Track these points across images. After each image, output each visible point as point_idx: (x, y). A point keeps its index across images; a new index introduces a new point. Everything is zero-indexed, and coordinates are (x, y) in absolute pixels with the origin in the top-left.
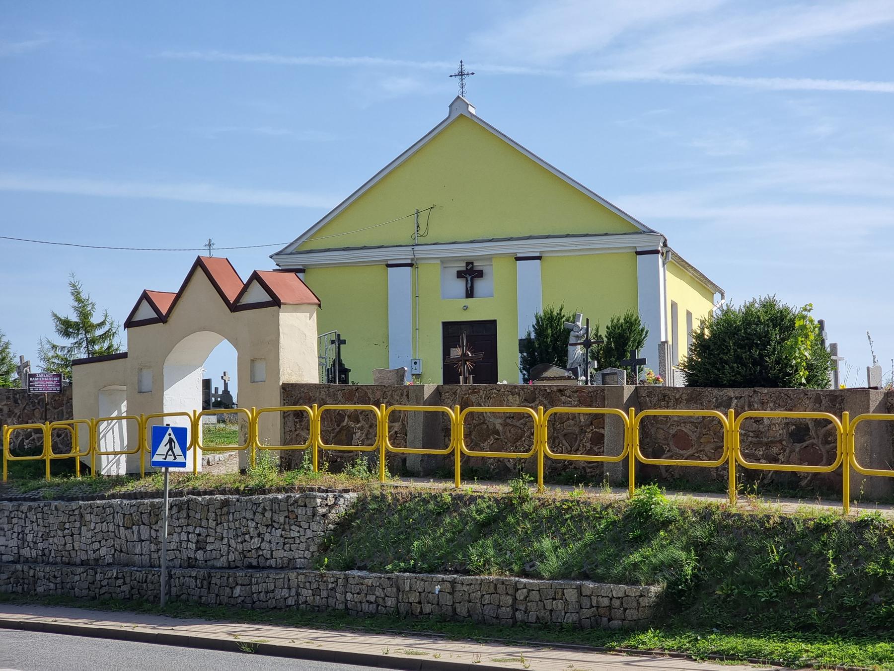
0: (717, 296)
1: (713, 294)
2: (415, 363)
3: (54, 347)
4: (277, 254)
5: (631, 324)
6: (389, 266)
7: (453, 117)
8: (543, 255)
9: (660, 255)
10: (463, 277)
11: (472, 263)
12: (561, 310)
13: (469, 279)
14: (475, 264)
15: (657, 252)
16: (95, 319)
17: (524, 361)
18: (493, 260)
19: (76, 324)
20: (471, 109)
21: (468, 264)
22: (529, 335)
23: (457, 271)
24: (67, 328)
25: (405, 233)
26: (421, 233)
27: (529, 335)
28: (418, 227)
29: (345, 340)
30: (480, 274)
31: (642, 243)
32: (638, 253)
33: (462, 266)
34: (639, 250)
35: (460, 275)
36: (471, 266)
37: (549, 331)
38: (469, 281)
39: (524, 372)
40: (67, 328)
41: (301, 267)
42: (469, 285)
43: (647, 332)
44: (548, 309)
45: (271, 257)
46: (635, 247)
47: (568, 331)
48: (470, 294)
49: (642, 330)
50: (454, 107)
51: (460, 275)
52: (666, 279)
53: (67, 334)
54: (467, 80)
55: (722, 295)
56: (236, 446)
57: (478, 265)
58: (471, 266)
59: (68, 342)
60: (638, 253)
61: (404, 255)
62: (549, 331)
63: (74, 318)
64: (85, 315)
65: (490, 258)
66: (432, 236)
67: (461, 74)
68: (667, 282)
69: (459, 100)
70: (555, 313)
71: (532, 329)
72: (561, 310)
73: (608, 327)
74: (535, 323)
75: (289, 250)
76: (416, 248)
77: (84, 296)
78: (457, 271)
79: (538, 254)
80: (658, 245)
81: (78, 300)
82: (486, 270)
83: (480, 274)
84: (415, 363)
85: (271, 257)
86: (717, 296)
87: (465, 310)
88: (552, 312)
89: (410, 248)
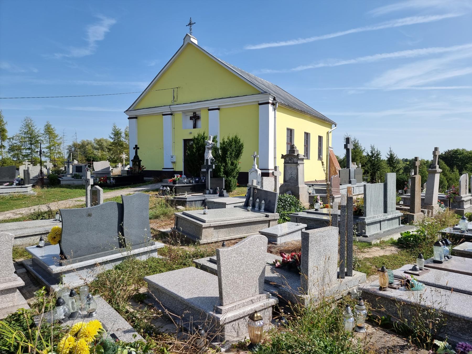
0: (333, 125)
1: (332, 125)
2: (172, 157)
4: (127, 111)
6: (209, 110)
8: (220, 108)
9: (270, 105)
10: (192, 119)
11: (196, 113)
13: (194, 120)
14: (197, 113)
18: (201, 111)
21: (194, 113)
23: (190, 117)
25: (169, 100)
26: (175, 100)
28: (174, 97)
31: (261, 98)
33: (191, 114)
35: (191, 118)
36: (195, 114)
38: (194, 121)
41: (135, 116)
42: (194, 123)
45: (124, 112)
46: (258, 101)
48: (195, 127)
52: (276, 117)
55: (336, 125)
56: (146, 178)
58: (195, 114)
60: (260, 104)
61: (167, 110)
67: (190, 24)
68: (276, 119)
69: (187, 36)
75: (131, 109)
76: (171, 106)
78: (190, 117)
79: (217, 107)
80: (269, 99)
84: (172, 157)
85: (124, 112)
86: (333, 125)
87: (190, 134)
89: (168, 107)
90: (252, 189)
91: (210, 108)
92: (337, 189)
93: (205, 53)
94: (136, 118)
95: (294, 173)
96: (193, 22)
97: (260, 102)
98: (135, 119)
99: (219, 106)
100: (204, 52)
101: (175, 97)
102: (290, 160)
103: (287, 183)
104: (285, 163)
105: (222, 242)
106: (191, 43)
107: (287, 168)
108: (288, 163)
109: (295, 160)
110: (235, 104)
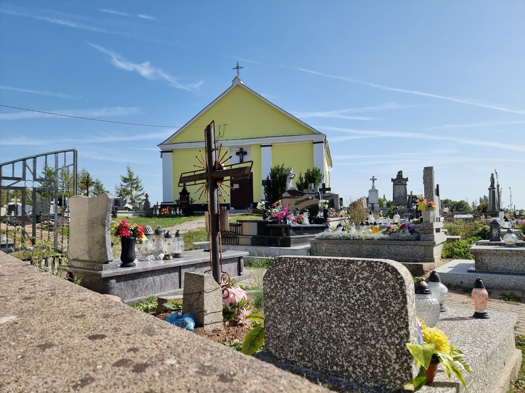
3: (122, 185)
5: (317, 172)
6: (262, 146)
7: (235, 85)
11: (242, 149)
12: (283, 166)
15: (322, 142)
16: (134, 177)
17: (266, 189)
19: (128, 179)
20: (241, 82)
21: (241, 149)
22: (268, 177)
24: (125, 180)
26: (221, 136)
27: (268, 177)
29: (407, 178)
30: (246, 153)
31: (316, 138)
32: (314, 143)
33: (238, 150)
34: (314, 141)
35: (237, 154)
37: (278, 176)
39: (266, 194)
40: (125, 180)
41: (171, 150)
42: (241, 158)
43: (323, 176)
44: (277, 166)
45: (158, 146)
46: (313, 140)
47: (286, 176)
49: (321, 175)
50: (235, 81)
51: (237, 154)
53: (125, 182)
54: (240, 70)
57: (245, 149)
59: (125, 184)
60: (314, 143)
62: (278, 176)
63: (128, 177)
64: (131, 176)
65: (250, 146)
66: (225, 137)
67: (238, 68)
70: (280, 168)
71: (269, 175)
72: (283, 166)
73: (305, 174)
74: (270, 172)
75: (166, 143)
77: (131, 171)
79: (270, 144)
81: (129, 172)
82: (248, 152)
83: (246, 153)
85: (158, 146)
88: (279, 167)
90: (411, 198)
91: (262, 145)
92: (210, 229)
93: (255, 94)
94: (172, 152)
95: (403, 191)
96: (240, 66)
97: (314, 141)
98: (171, 153)
99: (272, 143)
100: (255, 94)
101: (222, 134)
102: (399, 182)
103: (396, 200)
104: (394, 185)
105: (138, 265)
106: (241, 85)
107: (396, 189)
108: (397, 185)
109: (404, 182)
110: (288, 142)
